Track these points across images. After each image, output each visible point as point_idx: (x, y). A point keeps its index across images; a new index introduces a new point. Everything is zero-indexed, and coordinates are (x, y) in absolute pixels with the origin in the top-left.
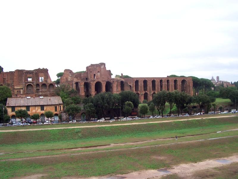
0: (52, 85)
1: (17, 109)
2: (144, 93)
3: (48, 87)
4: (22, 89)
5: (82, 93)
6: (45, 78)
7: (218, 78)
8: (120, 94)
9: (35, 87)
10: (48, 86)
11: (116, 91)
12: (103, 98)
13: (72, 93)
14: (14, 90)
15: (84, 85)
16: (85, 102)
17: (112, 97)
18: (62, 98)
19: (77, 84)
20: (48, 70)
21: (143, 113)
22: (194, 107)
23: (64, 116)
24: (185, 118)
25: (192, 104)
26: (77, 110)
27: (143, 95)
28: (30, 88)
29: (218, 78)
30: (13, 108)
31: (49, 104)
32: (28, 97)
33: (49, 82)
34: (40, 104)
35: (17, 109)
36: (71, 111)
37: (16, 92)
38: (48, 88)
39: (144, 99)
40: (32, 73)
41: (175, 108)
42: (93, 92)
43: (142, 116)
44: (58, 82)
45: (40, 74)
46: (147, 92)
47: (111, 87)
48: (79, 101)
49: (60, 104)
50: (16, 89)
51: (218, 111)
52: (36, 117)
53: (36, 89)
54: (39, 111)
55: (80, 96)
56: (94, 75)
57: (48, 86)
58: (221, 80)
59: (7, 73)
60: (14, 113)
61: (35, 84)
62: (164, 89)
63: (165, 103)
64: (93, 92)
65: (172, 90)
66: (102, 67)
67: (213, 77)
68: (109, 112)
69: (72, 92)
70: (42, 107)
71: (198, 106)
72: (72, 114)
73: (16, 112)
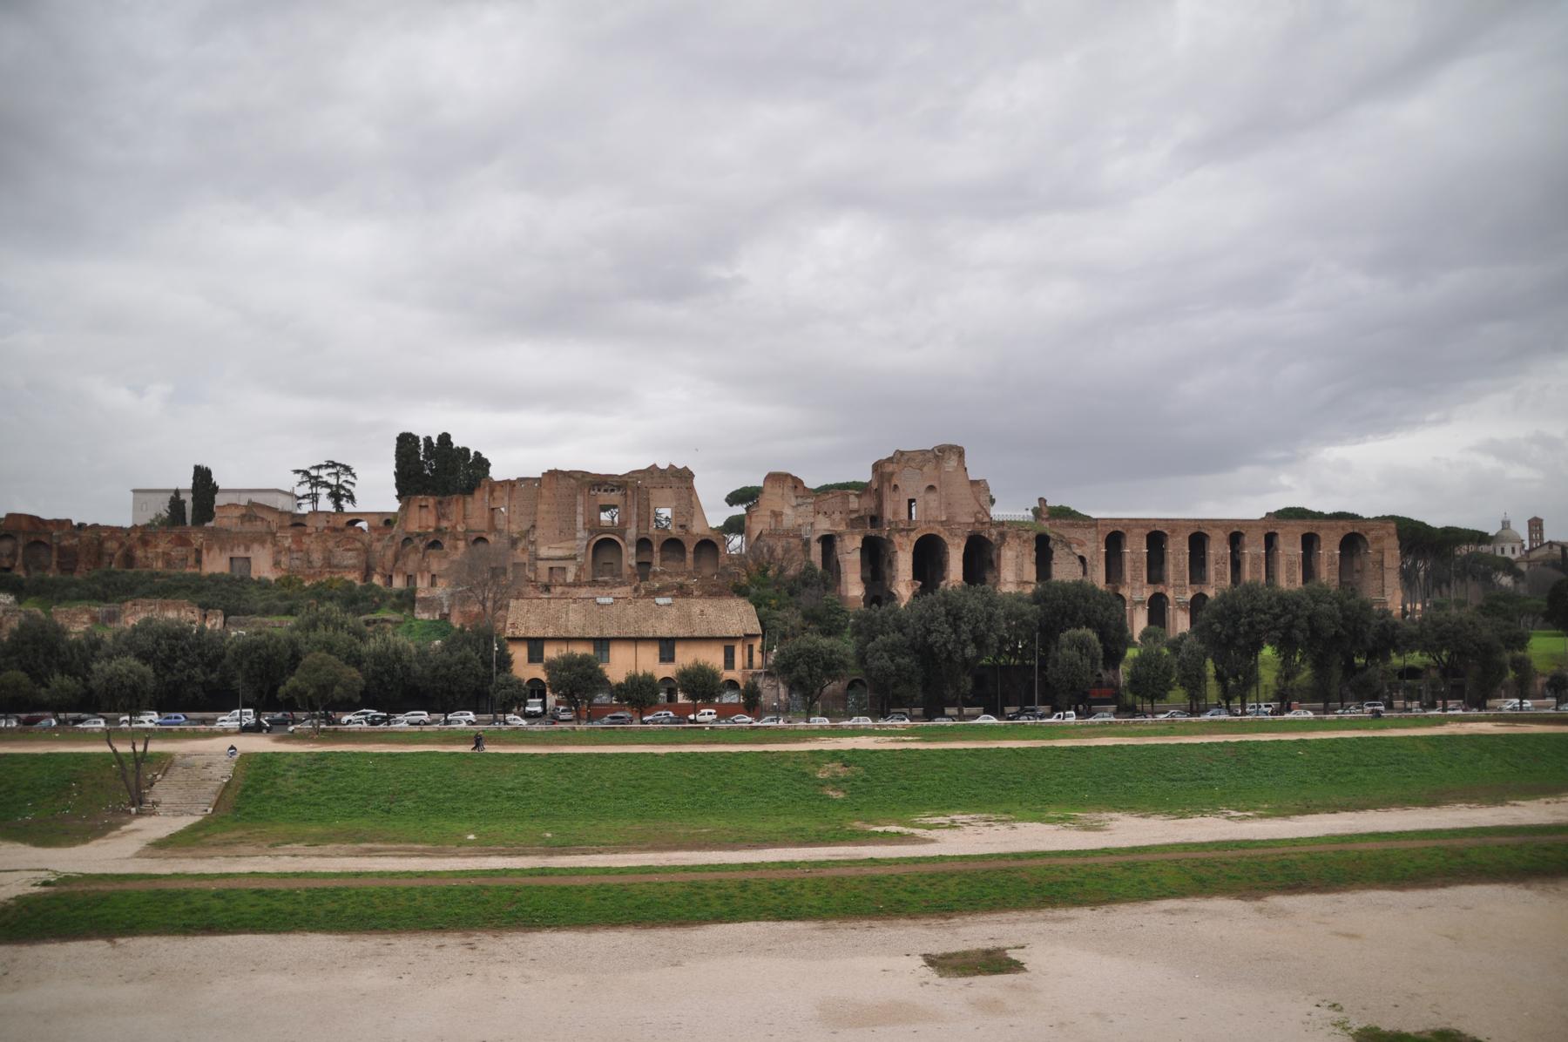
0: (708, 546)
1: (551, 652)
2: (1147, 593)
3: (690, 556)
4: (574, 558)
5: (854, 588)
6: (676, 513)
7: (1536, 525)
8: (1037, 598)
9: (633, 550)
10: (690, 548)
11: (1014, 574)
12: (954, 617)
13: (806, 584)
14: (540, 564)
15: (862, 550)
16: (866, 629)
17: (1000, 612)
18: (757, 607)
19: (828, 541)
20: (691, 475)
21: (1147, 690)
22: (1412, 672)
23: (773, 692)
24: (1349, 727)
25: (1396, 661)
26: (831, 667)
27: (1142, 603)
28: (607, 556)
29: (1536, 525)
30: (536, 646)
31: (696, 634)
32: (601, 600)
33: (697, 529)
34: (659, 634)
35: (551, 652)
36: (802, 670)
37: (546, 571)
38: (684, 555)
39: (1151, 621)
40: (619, 488)
41: (1305, 675)
42: (903, 586)
43: (1139, 706)
44: (734, 526)
45: (656, 494)
46: (1160, 589)
47: (991, 562)
48: (839, 626)
49: (748, 636)
50: (548, 559)
51: (1544, 697)
52: (639, 694)
53: (633, 563)
54: (648, 662)
55: (843, 599)
56: (911, 501)
57: (690, 548)
58: (1554, 539)
59: (510, 485)
60: (537, 671)
61: (632, 533)
62: (1252, 572)
63: (1258, 647)
64: (903, 586)
65: (1289, 580)
66: (951, 463)
67: (1506, 525)
68: (980, 682)
69: (807, 579)
70: (667, 647)
71: (1427, 666)
72: (807, 681)
73: (551, 667)
